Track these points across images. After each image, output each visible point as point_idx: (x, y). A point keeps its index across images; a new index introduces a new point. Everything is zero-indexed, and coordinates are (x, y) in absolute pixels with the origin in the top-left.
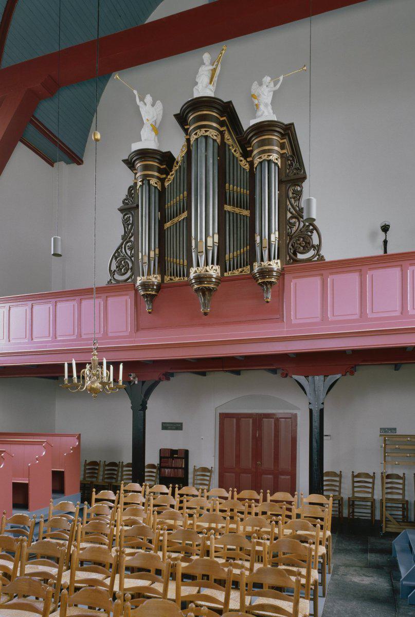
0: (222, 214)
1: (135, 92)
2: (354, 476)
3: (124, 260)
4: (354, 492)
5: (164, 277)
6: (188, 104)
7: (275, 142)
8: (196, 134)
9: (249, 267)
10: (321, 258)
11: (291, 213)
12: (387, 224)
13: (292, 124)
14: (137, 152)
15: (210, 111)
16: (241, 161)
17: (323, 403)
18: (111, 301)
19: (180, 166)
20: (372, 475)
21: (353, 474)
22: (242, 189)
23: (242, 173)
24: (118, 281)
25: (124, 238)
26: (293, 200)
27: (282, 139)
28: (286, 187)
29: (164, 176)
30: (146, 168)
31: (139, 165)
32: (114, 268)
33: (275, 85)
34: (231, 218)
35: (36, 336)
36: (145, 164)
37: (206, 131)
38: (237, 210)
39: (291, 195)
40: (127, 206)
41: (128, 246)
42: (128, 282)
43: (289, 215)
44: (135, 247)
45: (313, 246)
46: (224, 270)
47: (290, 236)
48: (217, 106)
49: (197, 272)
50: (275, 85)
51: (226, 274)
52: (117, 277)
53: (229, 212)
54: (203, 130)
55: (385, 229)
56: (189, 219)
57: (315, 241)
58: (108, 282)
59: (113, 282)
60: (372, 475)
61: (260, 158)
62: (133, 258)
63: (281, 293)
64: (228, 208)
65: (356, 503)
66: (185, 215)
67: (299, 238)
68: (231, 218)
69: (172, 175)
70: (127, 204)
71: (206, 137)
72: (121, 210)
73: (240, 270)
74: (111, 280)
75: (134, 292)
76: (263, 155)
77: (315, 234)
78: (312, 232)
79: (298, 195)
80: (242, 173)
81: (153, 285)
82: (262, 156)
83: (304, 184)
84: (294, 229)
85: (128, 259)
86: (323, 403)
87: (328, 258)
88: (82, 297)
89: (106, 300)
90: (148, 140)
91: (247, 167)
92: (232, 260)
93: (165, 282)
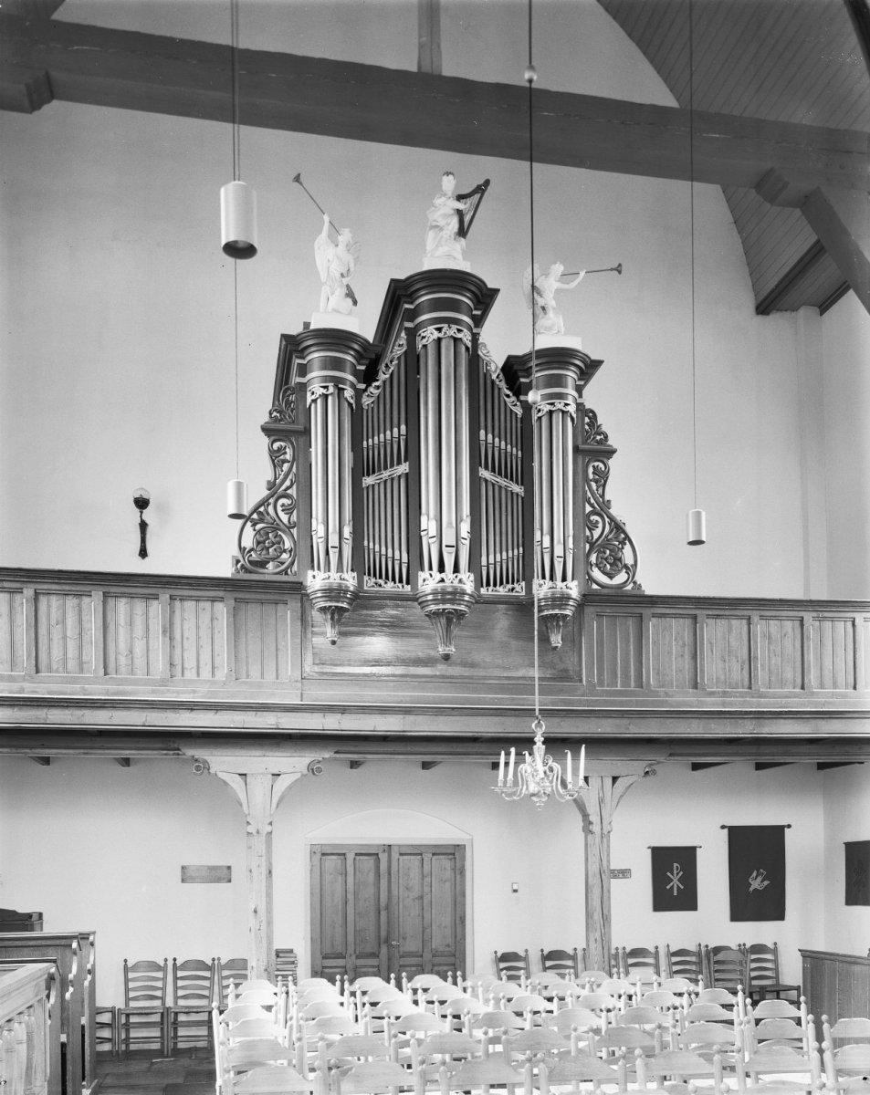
0: (475, 480)
2: (126, 969)
4: (128, 1000)
5: (363, 578)
8: (439, 330)
9: (523, 584)
11: (592, 505)
15: (452, 292)
16: (508, 396)
17: (271, 824)
19: (392, 375)
20: (772, 947)
21: (126, 966)
22: (509, 446)
23: (508, 418)
26: (594, 485)
27: (579, 379)
30: (336, 364)
31: (316, 355)
34: (490, 493)
35: (196, 675)
36: (335, 357)
37: (459, 331)
38: (502, 481)
39: (591, 476)
43: (588, 509)
45: (626, 566)
46: (479, 583)
48: (473, 288)
51: (483, 591)
53: (486, 481)
54: (454, 327)
55: (142, 503)
56: (413, 480)
57: (628, 559)
60: (653, 950)
61: (552, 404)
62: (294, 531)
64: (484, 473)
65: (182, 1018)
66: (404, 468)
68: (490, 493)
69: (378, 387)
71: (456, 340)
73: (510, 586)
76: (559, 401)
77: (627, 548)
78: (623, 543)
79: (602, 478)
80: (508, 418)
81: (346, 591)
82: (557, 401)
83: (611, 462)
84: (597, 533)
85: (284, 532)
86: (271, 824)
87: (649, 589)
88: (113, 590)
91: (519, 411)
92: (492, 567)
93: (365, 588)
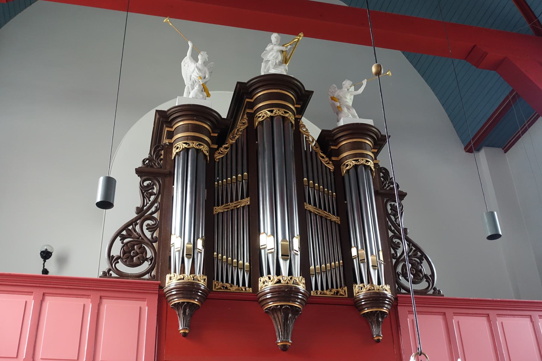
1: (190, 44)
3: (141, 243)
6: (262, 78)
7: (367, 147)
10: (437, 292)
12: (49, 250)
13: (238, 83)
14: (184, 107)
18: (108, 305)
24: (121, 275)
25: (140, 211)
26: (392, 217)
28: (383, 201)
29: (215, 146)
32: (117, 250)
33: (356, 90)
37: (286, 112)
40: (149, 169)
41: (148, 225)
42: (144, 279)
44: (163, 227)
45: (426, 276)
47: (394, 256)
48: (296, 89)
49: (282, 281)
50: (356, 90)
52: (121, 266)
58: (104, 273)
59: (114, 275)
63: (393, 325)
67: (406, 261)
70: (152, 166)
72: (139, 172)
74: (109, 270)
75: (156, 298)
76: (362, 158)
82: (360, 159)
89: (43, 300)
90: (191, 96)
